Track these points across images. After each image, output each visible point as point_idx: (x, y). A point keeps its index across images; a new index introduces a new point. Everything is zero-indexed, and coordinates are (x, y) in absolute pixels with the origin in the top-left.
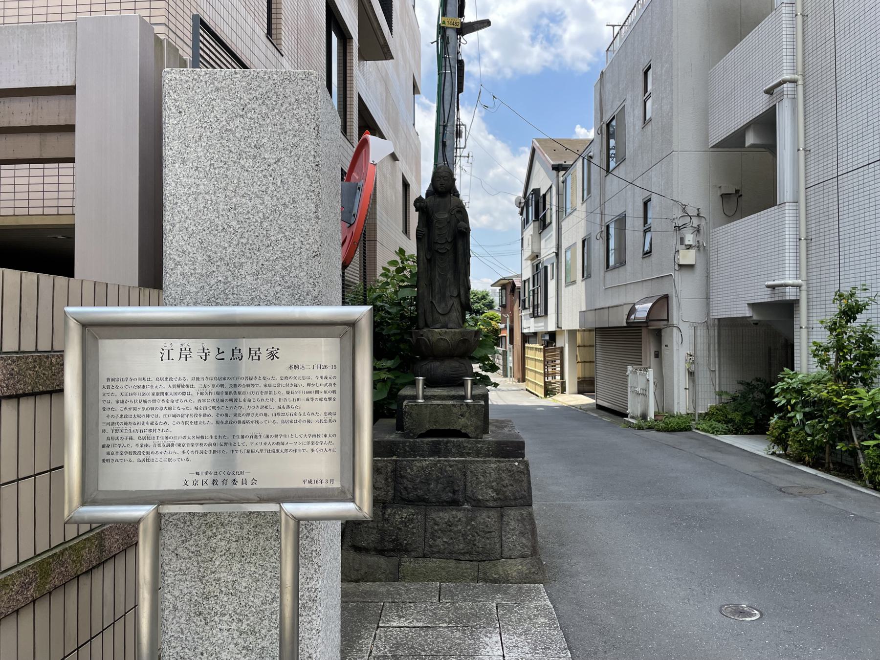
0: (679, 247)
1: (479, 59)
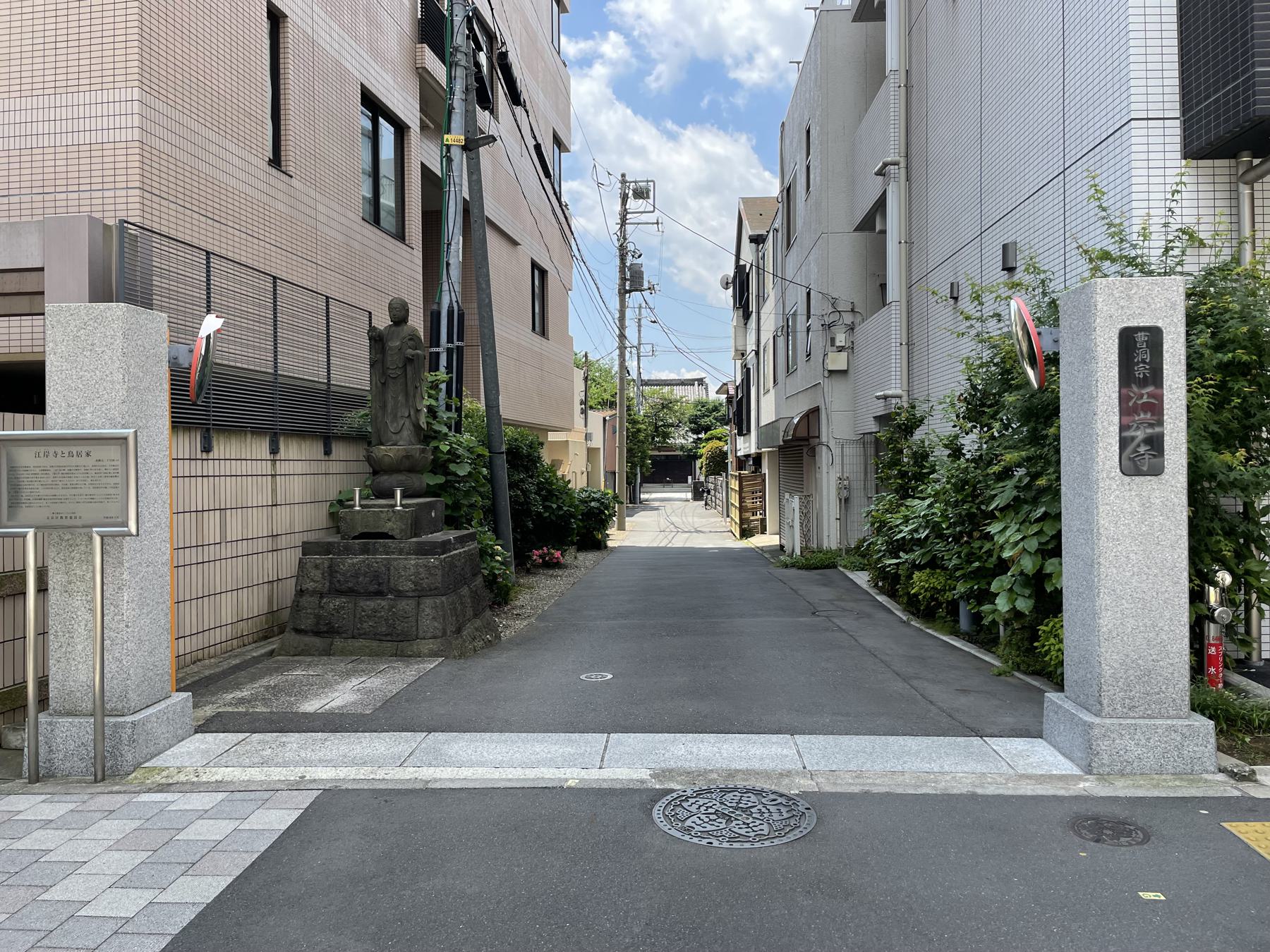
0: (829, 348)
1: (750, 59)
